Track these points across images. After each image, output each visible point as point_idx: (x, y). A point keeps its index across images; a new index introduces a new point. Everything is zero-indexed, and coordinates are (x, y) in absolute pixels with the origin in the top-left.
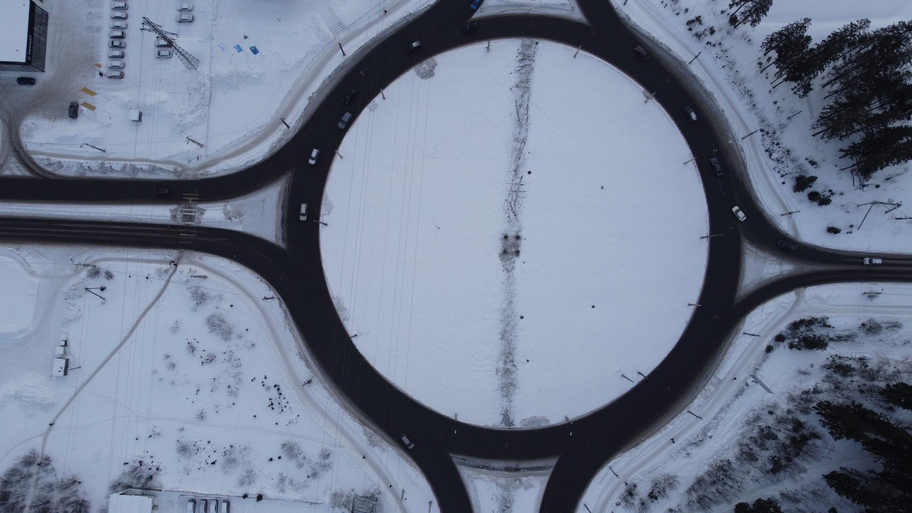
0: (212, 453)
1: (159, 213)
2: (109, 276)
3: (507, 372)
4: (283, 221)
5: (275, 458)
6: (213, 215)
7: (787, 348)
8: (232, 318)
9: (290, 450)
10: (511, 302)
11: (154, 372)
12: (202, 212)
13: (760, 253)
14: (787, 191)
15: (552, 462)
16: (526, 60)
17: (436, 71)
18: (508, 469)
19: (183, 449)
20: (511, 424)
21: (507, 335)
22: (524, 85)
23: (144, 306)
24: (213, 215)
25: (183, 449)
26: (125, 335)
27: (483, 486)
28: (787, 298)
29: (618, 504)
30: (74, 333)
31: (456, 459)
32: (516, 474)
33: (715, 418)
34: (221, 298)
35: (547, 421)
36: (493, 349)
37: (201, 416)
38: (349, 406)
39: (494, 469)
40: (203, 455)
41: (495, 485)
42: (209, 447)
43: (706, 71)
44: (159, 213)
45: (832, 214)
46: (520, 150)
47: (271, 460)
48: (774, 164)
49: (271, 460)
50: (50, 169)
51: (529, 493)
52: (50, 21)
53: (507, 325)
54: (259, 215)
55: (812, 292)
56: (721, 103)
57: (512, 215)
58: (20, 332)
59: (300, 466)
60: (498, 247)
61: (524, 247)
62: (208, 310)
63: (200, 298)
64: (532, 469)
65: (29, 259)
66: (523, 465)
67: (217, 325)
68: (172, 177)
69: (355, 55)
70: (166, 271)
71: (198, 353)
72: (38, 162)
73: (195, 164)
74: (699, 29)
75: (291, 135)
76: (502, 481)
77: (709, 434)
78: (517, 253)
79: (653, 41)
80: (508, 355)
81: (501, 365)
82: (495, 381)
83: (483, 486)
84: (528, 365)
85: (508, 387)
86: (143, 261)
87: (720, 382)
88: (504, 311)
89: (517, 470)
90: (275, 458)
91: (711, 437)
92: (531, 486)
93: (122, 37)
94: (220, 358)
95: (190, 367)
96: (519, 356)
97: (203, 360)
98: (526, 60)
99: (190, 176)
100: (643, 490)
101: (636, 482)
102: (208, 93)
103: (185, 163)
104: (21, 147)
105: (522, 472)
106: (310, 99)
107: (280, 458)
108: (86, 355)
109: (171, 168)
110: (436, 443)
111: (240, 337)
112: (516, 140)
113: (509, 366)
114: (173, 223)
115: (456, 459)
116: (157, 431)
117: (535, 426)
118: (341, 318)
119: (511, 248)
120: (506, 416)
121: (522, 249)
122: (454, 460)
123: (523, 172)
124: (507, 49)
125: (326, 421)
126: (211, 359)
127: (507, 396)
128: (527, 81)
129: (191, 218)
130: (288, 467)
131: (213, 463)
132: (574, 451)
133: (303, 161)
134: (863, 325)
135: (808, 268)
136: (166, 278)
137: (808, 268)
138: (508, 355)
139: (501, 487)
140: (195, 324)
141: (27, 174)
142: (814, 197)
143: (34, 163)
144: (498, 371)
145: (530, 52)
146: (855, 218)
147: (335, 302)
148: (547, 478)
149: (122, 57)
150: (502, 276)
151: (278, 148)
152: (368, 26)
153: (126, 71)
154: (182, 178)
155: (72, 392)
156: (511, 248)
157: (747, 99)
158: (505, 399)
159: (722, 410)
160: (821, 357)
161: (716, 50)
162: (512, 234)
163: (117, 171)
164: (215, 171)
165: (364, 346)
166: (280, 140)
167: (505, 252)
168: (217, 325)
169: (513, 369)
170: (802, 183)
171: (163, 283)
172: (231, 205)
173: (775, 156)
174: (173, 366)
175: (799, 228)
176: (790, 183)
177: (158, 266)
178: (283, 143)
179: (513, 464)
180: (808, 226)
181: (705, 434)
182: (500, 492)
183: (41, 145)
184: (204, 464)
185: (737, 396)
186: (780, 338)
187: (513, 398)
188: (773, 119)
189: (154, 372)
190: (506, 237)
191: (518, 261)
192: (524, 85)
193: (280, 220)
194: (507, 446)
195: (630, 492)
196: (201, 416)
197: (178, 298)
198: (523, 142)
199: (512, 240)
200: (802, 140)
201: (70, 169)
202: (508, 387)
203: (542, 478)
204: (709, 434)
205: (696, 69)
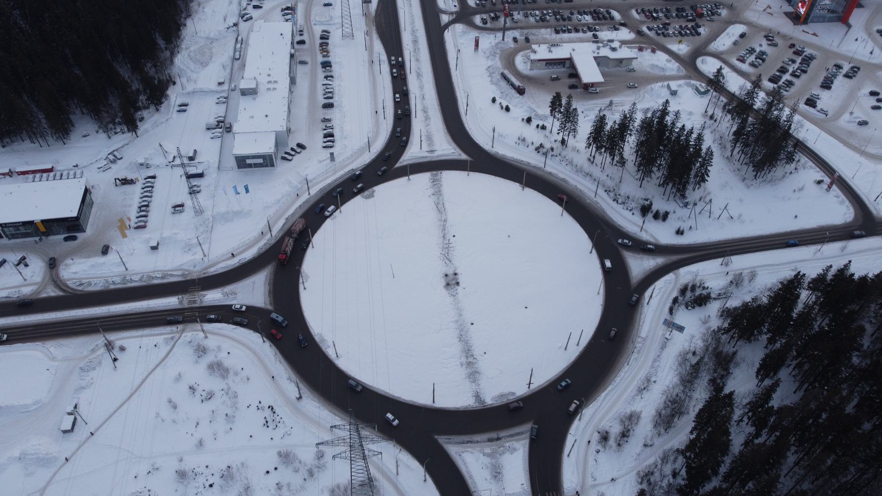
0: (210, 477)
1: (171, 302)
2: (122, 349)
3: (469, 364)
4: (270, 293)
5: (272, 470)
6: (213, 297)
7: (653, 220)
8: (228, 362)
9: (286, 457)
10: (461, 315)
11: (158, 415)
12: (204, 296)
13: (636, 255)
14: (637, 218)
15: (527, 427)
16: (436, 183)
17: (375, 194)
18: (490, 440)
19: (182, 475)
20: (484, 402)
21: (463, 339)
22: (440, 208)
23: (152, 367)
24: (213, 297)
25: (182, 475)
26: (134, 388)
27: (471, 459)
28: (670, 277)
29: (598, 452)
30: (84, 400)
31: (442, 440)
32: (498, 442)
33: (652, 367)
34: (219, 348)
35: (513, 394)
36: (456, 349)
37: (201, 443)
38: (337, 413)
39: (477, 442)
40: (201, 480)
41: (481, 455)
42: (206, 472)
43: (555, 169)
44: (171, 302)
45: (673, 224)
46: (444, 226)
47: (268, 472)
48: (622, 206)
49: (268, 472)
50: (80, 288)
51: (516, 457)
52: (94, 206)
53: (462, 330)
54: (254, 292)
55: (683, 271)
56: (573, 182)
57: (448, 262)
58: (34, 404)
59: (297, 471)
60: (443, 282)
61: (461, 279)
62: (209, 358)
63: (201, 351)
64: (512, 436)
65: (52, 349)
66: (502, 434)
67: (218, 369)
68: (180, 279)
69: (316, 194)
70: (172, 338)
71: (197, 394)
72: (71, 285)
73: (198, 268)
74: (541, 150)
75: (273, 242)
76: (488, 450)
77: (653, 379)
78: (458, 284)
79: (516, 161)
80: (468, 352)
81: (464, 360)
82: (463, 372)
83: (471, 459)
84: (485, 356)
85: (474, 375)
86: (154, 335)
87: (644, 339)
88: (457, 321)
89: (498, 439)
90: (272, 470)
91: (655, 382)
92: (515, 450)
93: (147, 206)
94: (218, 394)
95: (193, 408)
96: (477, 351)
97: (203, 398)
98: (436, 183)
99: (195, 276)
100: (615, 430)
101: (607, 428)
102: (210, 225)
103: (191, 268)
104: (59, 278)
105: (503, 440)
106: (287, 219)
107: (276, 469)
108: (91, 413)
109: (180, 273)
110: (423, 431)
111: (236, 374)
112: (440, 220)
113: (470, 360)
114: (180, 307)
115: (442, 440)
116: (156, 466)
117: (505, 401)
118: (323, 349)
119: (452, 282)
120: (477, 396)
121: (460, 280)
122: (440, 441)
123: (449, 236)
124: (423, 179)
125: (315, 422)
126: (210, 396)
127: (474, 381)
128: (440, 191)
129: (194, 302)
130: (285, 475)
131: (211, 486)
132: (544, 416)
133: (284, 258)
134: (731, 282)
135: (674, 258)
136: (173, 343)
137: (674, 258)
138: (468, 352)
139: (488, 455)
140: (197, 373)
141: (61, 294)
142: (656, 216)
143: (68, 287)
144: (462, 365)
145: (438, 177)
146: (691, 222)
147: (317, 338)
148: (526, 442)
149: (146, 216)
150: (450, 300)
151: (264, 250)
152: (326, 178)
153: (148, 224)
154: (188, 278)
155: (76, 445)
156: (452, 282)
157: (588, 178)
158: (474, 385)
159: (655, 361)
160: (714, 308)
161: (558, 158)
162: (450, 272)
163: (136, 282)
164: (213, 271)
165: (343, 364)
166: (265, 244)
167: (448, 284)
168: (218, 369)
169: (474, 361)
170: (645, 210)
171: (169, 348)
172: (228, 289)
173: (620, 201)
174: (175, 407)
175: (656, 236)
176: (638, 213)
177: (166, 336)
178: (268, 246)
179: (493, 435)
180: (662, 234)
181: (648, 381)
182: (487, 460)
183: (76, 273)
184: (201, 489)
185: (662, 348)
186: (675, 301)
187: (480, 382)
188: (610, 183)
189: (158, 415)
190: (446, 275)
191: (460, 289)
192: (440, 208)
193: (267, 292)
194: (485, 421)
195: (605, 438)
196: (201, 443)
197: (183, 354)
198: (445, 221)
199: (451, 277)
200: (631, 187)
201: (97, 286)
202: (474, 375)
203: (523, 442)
204: (653, 379)
205: (548, 169)
